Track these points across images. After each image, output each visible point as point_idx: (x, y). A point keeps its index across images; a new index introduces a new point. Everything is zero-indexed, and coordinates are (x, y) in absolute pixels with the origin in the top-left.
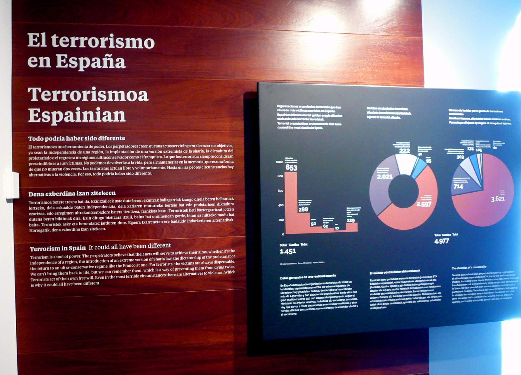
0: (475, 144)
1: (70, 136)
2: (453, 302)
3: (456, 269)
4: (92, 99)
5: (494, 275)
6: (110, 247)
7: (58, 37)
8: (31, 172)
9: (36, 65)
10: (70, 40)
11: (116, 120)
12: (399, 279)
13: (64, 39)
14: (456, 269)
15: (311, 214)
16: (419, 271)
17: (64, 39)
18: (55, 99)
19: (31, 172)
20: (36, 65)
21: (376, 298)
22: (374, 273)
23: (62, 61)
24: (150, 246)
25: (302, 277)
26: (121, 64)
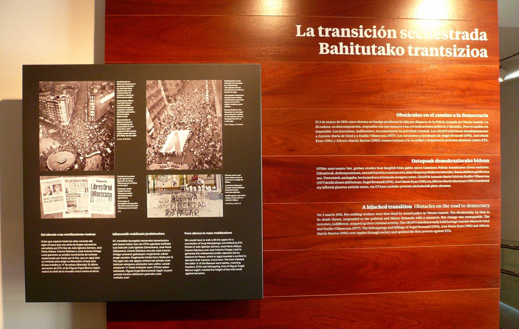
11: (341, 53)
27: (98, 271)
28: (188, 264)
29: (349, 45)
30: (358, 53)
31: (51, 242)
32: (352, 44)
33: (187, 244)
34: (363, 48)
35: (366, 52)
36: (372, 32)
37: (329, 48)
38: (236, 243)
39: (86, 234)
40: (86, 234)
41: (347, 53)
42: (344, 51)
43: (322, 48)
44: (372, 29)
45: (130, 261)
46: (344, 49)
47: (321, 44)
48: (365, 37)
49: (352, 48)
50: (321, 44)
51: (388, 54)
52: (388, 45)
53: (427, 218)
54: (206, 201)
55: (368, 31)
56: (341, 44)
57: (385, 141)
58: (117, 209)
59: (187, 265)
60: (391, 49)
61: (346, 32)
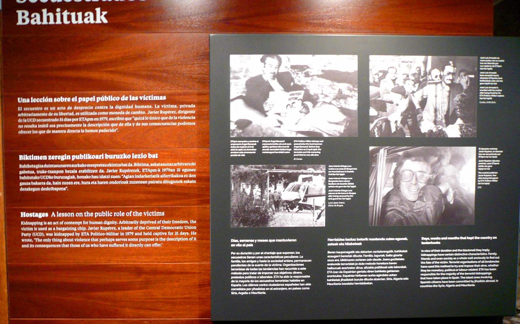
0: (327, 170)
1: (136, 153)
2: (22, 189)
6: (94, 215)
7: (69, 13)
8: (20, 129)
11: (45, 22)
12: (453, 251)
19: (20, 129)
21: (290, 261)
24: (129, 214)
26: (101, 18)
27: (308, 288)
28: (424, 263)
29: (55, 13)
30: (66, 22)
31: (281, 253)
32: (58, 10)
34: (73, 14)
35: (77, 19)
37: (30, 17)
39: (277, 240)
40: (277, 240)
41: (52, 22)
42: (48, 20)
46: (48, 17)
47: (20, 12)
49: (58, 15)
50: (20, 12)
51: (98, 21)
52: (98, 10)
53: (31, 229)
54: (277, 190)
56: (44, 11)
58: (477, 185)
59: (423, 265)
60: (101, 14)
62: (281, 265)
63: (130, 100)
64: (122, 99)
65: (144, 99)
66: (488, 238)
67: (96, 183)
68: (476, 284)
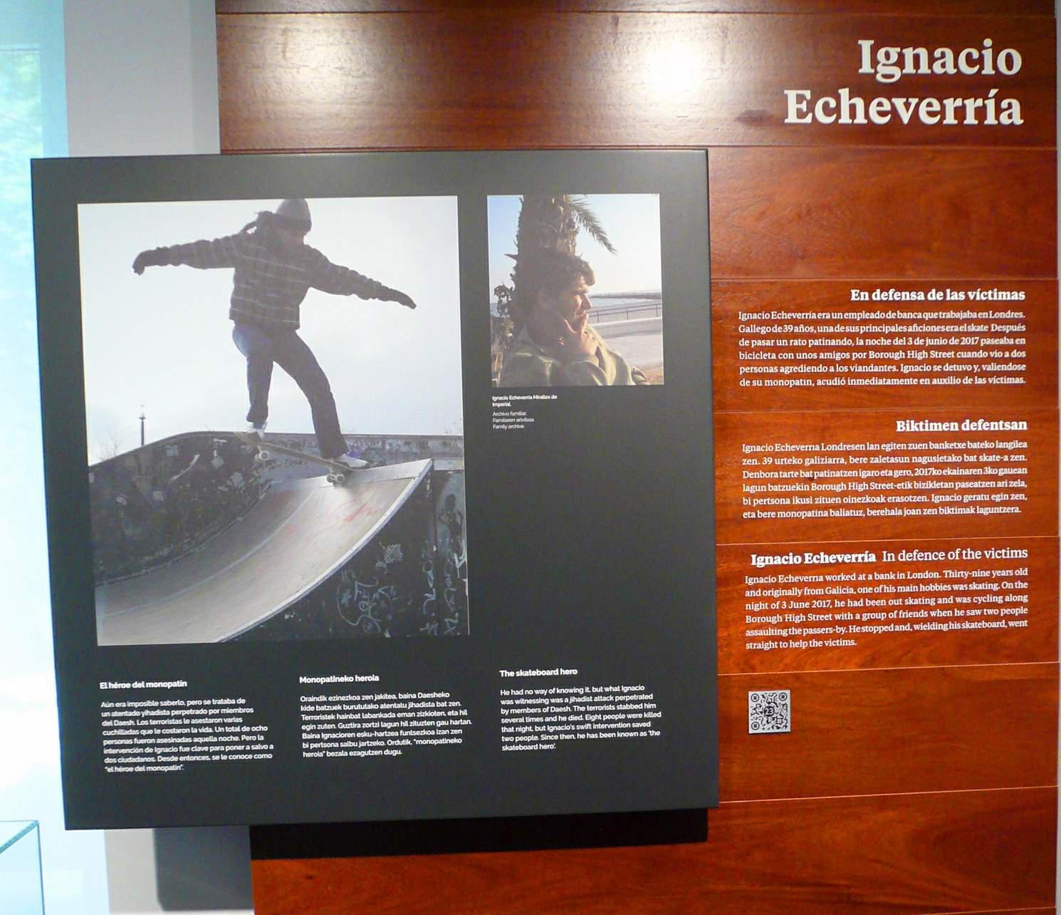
3: (512, 674)
4: (985, 118)
5: (840, 375)
9: (939, 117)
10: (943, 107)
13: (880, 104)
14: (512, 674)
15: (995, 101)
16: (183, 684)
17: (880, 104)
18: (950, 119)
20: (939, 117)
22: (527, 674)
23: (799, 106)
24: (955, 555)
25: (350, 679)
33: (110, 733)
36: (981, 57)
38: (246, 729)
43: (899, 426)
44: (981, 48)
45: (450, 713)
48: (959, 73)
55: (969, 56)
57: (923, 627)
61: (916, 58)
62: (236, 739)
63: (948, 298)
64: (929, 298)
65: (978, 298)
66: (362, 679)
67: (900, 513)
68: (558, 742)
